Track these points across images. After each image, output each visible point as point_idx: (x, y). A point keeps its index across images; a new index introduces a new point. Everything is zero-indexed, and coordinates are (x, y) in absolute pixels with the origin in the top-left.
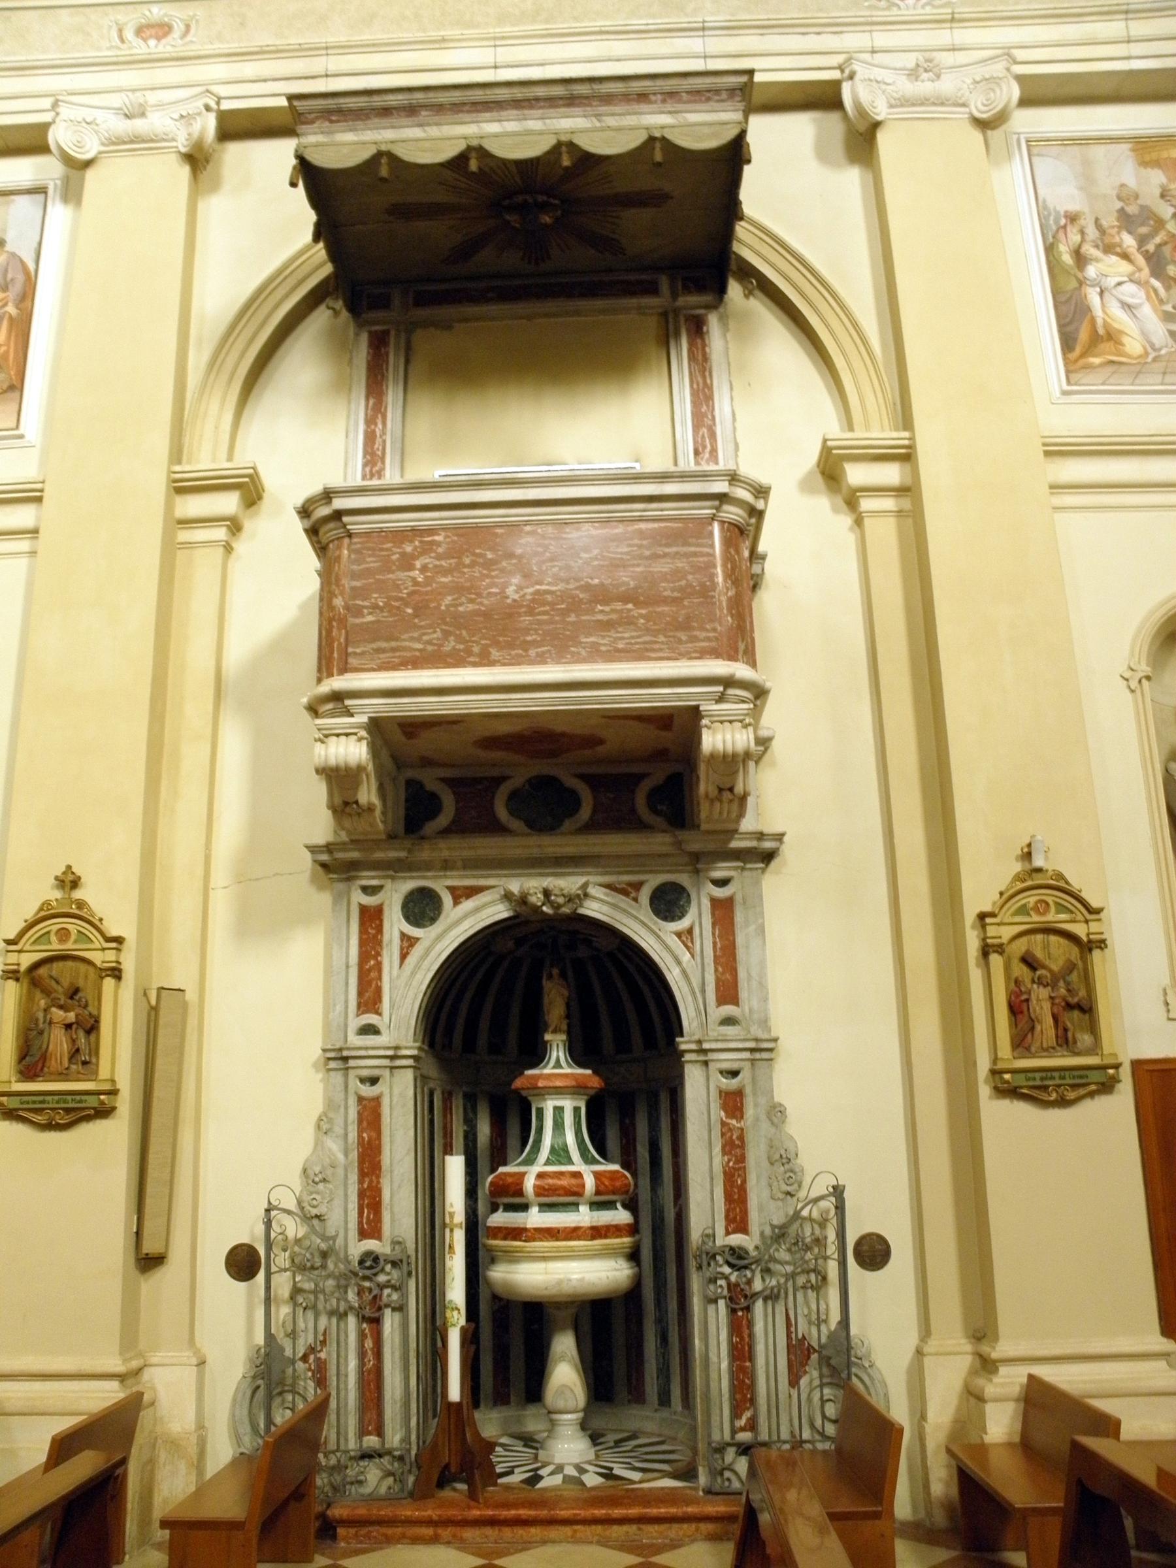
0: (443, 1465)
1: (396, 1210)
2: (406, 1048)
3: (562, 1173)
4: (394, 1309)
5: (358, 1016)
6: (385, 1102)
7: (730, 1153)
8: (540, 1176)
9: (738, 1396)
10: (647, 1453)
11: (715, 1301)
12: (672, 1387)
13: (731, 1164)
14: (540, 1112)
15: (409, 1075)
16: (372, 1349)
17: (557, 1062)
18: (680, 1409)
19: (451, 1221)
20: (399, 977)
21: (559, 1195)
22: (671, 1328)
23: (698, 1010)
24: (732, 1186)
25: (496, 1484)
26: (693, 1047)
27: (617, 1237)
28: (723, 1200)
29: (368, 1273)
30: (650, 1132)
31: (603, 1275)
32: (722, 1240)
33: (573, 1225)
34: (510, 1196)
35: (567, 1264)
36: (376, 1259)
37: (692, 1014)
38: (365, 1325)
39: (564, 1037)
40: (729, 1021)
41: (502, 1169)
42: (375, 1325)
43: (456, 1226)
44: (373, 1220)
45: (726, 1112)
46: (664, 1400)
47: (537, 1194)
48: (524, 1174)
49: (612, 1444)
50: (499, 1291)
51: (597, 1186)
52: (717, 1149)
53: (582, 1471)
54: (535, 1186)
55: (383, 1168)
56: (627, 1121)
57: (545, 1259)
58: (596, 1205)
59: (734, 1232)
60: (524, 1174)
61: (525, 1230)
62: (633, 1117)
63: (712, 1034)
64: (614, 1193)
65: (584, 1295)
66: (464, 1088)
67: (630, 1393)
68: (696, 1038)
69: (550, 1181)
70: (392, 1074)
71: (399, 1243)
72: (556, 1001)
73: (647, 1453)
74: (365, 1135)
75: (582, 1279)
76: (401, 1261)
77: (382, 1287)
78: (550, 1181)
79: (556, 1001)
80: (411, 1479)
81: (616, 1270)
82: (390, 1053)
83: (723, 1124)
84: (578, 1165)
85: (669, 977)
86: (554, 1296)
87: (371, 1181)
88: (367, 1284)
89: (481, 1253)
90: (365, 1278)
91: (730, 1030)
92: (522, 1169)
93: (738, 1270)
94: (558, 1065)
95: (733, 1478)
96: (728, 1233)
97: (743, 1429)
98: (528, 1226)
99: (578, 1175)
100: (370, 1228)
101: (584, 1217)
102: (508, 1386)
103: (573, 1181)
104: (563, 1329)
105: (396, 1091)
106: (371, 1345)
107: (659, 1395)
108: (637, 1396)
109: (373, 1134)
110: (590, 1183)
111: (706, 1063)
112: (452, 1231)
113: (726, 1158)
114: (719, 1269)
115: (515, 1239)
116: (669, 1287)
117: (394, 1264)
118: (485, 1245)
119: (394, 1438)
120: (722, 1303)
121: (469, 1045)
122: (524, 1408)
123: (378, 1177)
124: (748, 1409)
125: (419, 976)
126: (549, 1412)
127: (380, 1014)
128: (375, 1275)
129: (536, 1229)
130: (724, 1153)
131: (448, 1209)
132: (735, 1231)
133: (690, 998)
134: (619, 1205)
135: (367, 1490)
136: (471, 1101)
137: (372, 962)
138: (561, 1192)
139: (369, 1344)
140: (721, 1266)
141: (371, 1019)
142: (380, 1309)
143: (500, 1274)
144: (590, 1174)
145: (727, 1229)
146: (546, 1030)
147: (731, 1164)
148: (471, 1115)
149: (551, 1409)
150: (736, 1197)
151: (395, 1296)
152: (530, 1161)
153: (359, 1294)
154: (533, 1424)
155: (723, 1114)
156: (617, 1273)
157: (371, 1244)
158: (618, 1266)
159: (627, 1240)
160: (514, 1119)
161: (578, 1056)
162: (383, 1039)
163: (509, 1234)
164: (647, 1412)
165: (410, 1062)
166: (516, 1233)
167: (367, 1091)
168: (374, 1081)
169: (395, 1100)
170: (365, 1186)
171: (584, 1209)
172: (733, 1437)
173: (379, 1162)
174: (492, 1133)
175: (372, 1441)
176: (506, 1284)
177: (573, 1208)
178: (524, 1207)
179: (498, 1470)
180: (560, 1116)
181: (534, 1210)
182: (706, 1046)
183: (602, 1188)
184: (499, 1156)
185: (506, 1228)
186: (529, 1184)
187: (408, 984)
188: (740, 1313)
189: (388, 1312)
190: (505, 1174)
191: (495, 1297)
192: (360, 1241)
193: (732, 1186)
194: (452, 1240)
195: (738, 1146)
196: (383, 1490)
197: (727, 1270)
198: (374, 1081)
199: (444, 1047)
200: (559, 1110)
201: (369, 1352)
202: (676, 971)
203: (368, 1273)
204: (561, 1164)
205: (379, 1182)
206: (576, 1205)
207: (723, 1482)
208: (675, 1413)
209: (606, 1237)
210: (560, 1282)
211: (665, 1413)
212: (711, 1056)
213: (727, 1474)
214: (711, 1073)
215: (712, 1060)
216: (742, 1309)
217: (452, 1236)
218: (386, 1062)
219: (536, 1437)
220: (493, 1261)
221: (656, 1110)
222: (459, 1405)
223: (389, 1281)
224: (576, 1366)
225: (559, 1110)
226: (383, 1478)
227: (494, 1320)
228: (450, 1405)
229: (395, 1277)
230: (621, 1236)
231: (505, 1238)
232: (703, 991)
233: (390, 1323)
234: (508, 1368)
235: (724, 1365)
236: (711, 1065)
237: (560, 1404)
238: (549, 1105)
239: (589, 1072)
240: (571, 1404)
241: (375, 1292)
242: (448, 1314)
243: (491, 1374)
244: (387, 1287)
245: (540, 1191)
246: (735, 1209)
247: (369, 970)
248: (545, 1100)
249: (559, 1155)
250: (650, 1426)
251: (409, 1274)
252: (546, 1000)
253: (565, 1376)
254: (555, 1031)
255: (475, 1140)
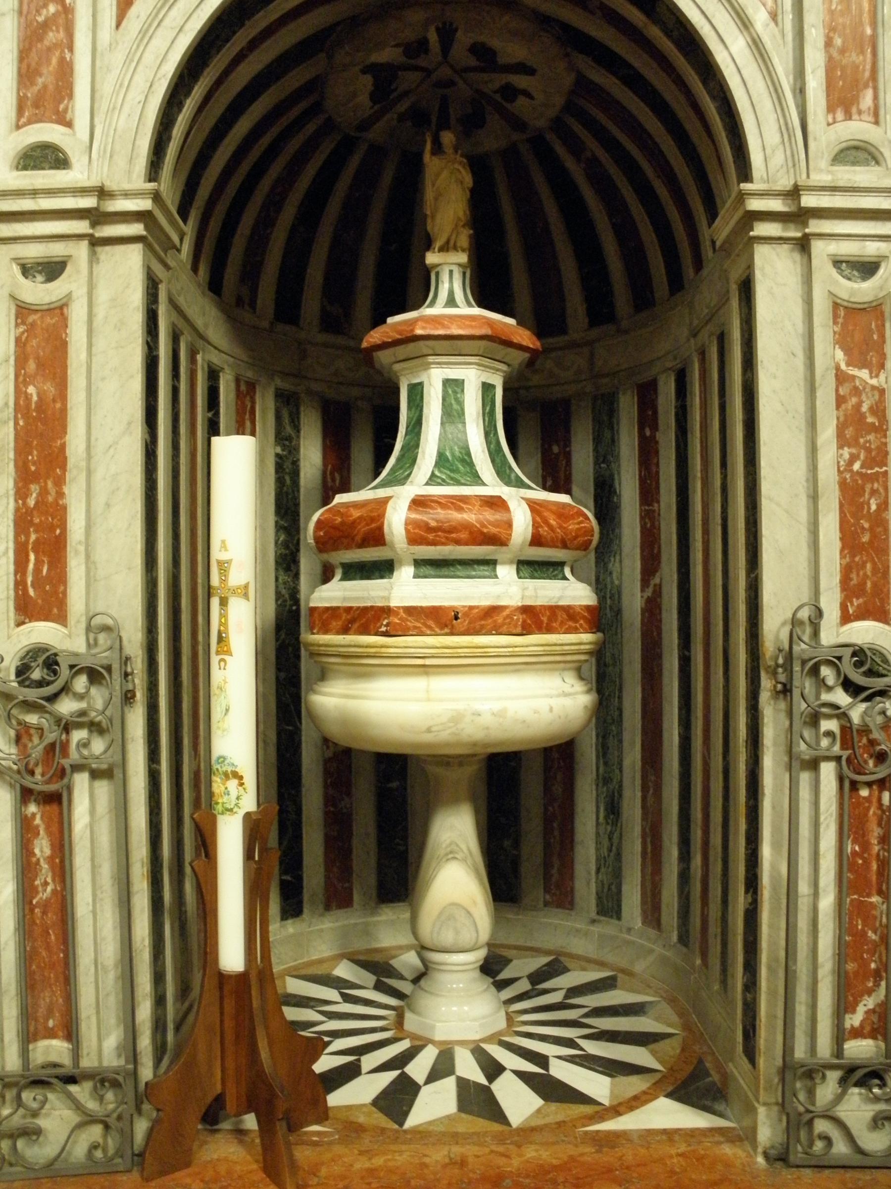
0: (209, 1099)
1: (100, 554)
2: (126, 195)
3: (464, 499)
4: (95, 775)
5: (18, 127)
6: (77, 314)
7: (853, 442)
8: (418, 503)
9: (851, 966)
10: (599, 1012)
11: (813, 765)
12: (625, 888)
13: (857, 466)
14: (417, 392)
15: (134, 256)
16: (50, 860)
17: (450, 300)
18: (638, 923)
19: (224, 580)
20: (111, 47)
21: (458, 542)
22: (627, 793)
23: (785, 129)
24: (857, 515)
25: (323, 1114)
26: (776, 205)
27: (568, 631)
28: (838, 545)
29: (32, 694)
30: (597, 463)
31: (543, 704)
32: (833, 633)
33: (486, 603)
34: (361, 548)
35: (471, 675)
36: (51, 663)
37: (773, 136)
38: (32, 808)
39: (463, 258)
40: (858, 153)
41: (340, 499)
42: (54, 808)
43: (234, 592)
44: (49, 579)
45: (847, 351)
46: (609, 906)
47: (413, 540)
48: (385, 501)
49: (524, 985)
50: (335, 731)
51: (535, 525)
52: (827, 433)
53: (494, 1069)
54: (407, 523)
55: (71, 462)
56: (556, 449)
57: (425, 670)
58: (531, 568)
59: (861, 616)
60: (385, 501)
61: (386, 611)
62: (566, 442)
63: (821, 177)
64: (565, 545)
65: (501, 743)
66: (278, 382)
67: (547, 890)
68: (785, 183)
69: (441, 514)
70: (93, 258)
71: (106, 629)
72: (447, 194)
73: (599, 1012)
74: (31, 390)
75: (501, 714)
76: (109, 669)
77: (67, 727)
78: (441, 514)
79: (447, 194)
80: (141, 1127)
81: (566, 695)
82: (88, 202)
83: (841, 378)
84: (493, 487)
85: (721, 57)
86: (448, 744)
87: (44, 492)
88: (32, 719)
89: (305, 664)
90: (29, 706)
91: (862, 175)
92: (381, 493)
93: (868, 699)
94: (451, 302)
95: (835, 1134)
96: (846, 618)
97: (857, 1033)
98: (394, 603)
99: (496, 503)
100: (40, 599)
101: (507, 588)
102: (349, 880)
103: (489, 515)
104: (455, 801)
105: (103, 295)
106: (48, 852)
107: (599, 898)
108: (562, 896)
109: (50, 388)
110: (522, 522)
111: (803, 245)
112: (224, 602)
113: (846, 453)
114: (825, 697)
115: (365, 630)
116: (626, 724)
117: (95, 676)
118: (308, 645)
119: (102, 1045)
120: (828, 770)
121: (288, 309)
122: (374, 912)
123: (60, 482)
124: (870, 992)
125: (159, 43)
126: (423, 948)
127: (69, 124)
128: (53, 698)
129: (411, 611)
130: (842, 440)
131: (217, 554)
132: (862, 615)
133: (766, 105)
134: (567, 571)
135: (39, 1153)
136: (288, 405)
137: (52, 9)
138: (464, 535)
139: (42, 847)
140: (830, 689)
141: (48, 132)
142: (62, 773)
143: (335, 700)
144: (521, 506)
145: (844, 608)
146: (428, 245)
147: (857, 466)
148: (289, 430)
149: (427, 942)
150: (866, 538)
151: (98, 746)
152: (400, 479)
153: (18, 740)
154: (388, 932)
155: (840, 355)
156: (568, 702)
157: (43, 632)
158: (567, 688)
159: (586, 639)
160: (364, 422)
161: (488, 289)
162: (77, 174)
163: (352, 621)
164: (575, 922)
165: (137, 229)
166: (367, 619)
167: (37, 292)
168: (52, 270)
169: (100, 312)
170: (31, 502)
171: (506, 572)
172: (839, 1052)
173: (63, 447)
174: (325, 465)
175: (53, 1050)
176: (346, 721)
177: (483, 570)
178: (384, 569)
179: (324, 1064)
180: (453, 388)
181: (405, 573)
182: (808, 201)
183: (544, 531)
184: (338, 478)
185: (349, 609)
186: (397, 520)
187: (133, 60)
188: (864, 793)
189: (81, 780)
190: (347, 505)
191: (326, 741)
192: (19, 624)
193: (857, 515)
194: (224, 624)
195: (873, 429)
196: (79, 1151)
197: (841, 698)
198: (52, 270)
199: (239, 302)
200: (453, 387)
201: (45, 866)
202: (738, 44)
203: (32, 694)
204: (458, 483)
205: (61, 494)
206: (491, 563)
207: (811, 1144)
208: (629, 930)
209: (549, 630)
210: (457, 719)
211: (608, 927)
212: (815, 226)
213: (821, 1126)
214: (815, 262)
215: (821, 236)
216: (869, 784)
217: (223, 615)
218: (81, 226)
219: (394, 963)
220: (323, 675)
221: (611, 427)
222: (242, 978)
223: (83, 713)
224: (477, 871)
225: (453, 387)
226: (80, 1126)
227: (327, 772)
228: (222, 978)
229: (99, 704)
230: (575, 630)
231: (345, 630)
232: (800, 91)
233: (87, 803)
234: (350, 851)
235: (827, 902)
236: (819, 248)
237: (447, 937)
238: (434, 378)
239: (511, 321)
240: (467, 937)
241: (51, 736)
242: (218, 786)
243: (321, 859)
244: (79, 726)
245: (419, 534)
246: (863, 565)
247: (45, 26)
248: (427, 367)
249: (456, 471)
250: (579, 946)
251: (128, 697)
252: (429, 194)
253: (455, 881)
254: (445, 248)
255: (295, 473)
